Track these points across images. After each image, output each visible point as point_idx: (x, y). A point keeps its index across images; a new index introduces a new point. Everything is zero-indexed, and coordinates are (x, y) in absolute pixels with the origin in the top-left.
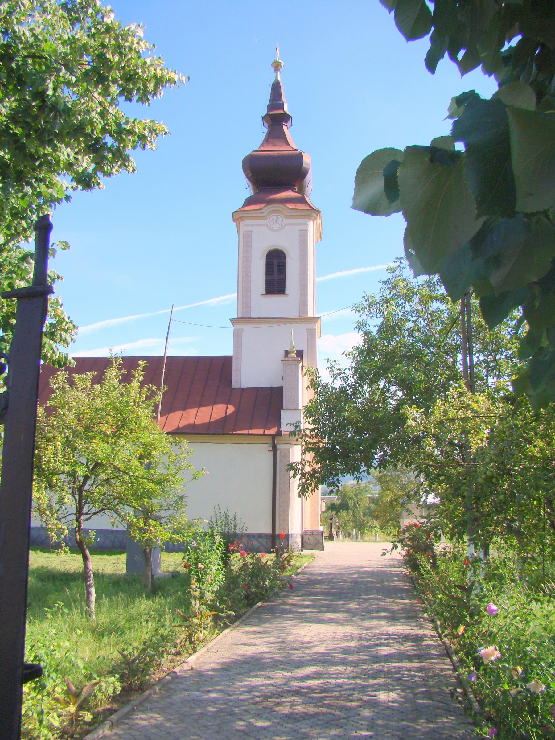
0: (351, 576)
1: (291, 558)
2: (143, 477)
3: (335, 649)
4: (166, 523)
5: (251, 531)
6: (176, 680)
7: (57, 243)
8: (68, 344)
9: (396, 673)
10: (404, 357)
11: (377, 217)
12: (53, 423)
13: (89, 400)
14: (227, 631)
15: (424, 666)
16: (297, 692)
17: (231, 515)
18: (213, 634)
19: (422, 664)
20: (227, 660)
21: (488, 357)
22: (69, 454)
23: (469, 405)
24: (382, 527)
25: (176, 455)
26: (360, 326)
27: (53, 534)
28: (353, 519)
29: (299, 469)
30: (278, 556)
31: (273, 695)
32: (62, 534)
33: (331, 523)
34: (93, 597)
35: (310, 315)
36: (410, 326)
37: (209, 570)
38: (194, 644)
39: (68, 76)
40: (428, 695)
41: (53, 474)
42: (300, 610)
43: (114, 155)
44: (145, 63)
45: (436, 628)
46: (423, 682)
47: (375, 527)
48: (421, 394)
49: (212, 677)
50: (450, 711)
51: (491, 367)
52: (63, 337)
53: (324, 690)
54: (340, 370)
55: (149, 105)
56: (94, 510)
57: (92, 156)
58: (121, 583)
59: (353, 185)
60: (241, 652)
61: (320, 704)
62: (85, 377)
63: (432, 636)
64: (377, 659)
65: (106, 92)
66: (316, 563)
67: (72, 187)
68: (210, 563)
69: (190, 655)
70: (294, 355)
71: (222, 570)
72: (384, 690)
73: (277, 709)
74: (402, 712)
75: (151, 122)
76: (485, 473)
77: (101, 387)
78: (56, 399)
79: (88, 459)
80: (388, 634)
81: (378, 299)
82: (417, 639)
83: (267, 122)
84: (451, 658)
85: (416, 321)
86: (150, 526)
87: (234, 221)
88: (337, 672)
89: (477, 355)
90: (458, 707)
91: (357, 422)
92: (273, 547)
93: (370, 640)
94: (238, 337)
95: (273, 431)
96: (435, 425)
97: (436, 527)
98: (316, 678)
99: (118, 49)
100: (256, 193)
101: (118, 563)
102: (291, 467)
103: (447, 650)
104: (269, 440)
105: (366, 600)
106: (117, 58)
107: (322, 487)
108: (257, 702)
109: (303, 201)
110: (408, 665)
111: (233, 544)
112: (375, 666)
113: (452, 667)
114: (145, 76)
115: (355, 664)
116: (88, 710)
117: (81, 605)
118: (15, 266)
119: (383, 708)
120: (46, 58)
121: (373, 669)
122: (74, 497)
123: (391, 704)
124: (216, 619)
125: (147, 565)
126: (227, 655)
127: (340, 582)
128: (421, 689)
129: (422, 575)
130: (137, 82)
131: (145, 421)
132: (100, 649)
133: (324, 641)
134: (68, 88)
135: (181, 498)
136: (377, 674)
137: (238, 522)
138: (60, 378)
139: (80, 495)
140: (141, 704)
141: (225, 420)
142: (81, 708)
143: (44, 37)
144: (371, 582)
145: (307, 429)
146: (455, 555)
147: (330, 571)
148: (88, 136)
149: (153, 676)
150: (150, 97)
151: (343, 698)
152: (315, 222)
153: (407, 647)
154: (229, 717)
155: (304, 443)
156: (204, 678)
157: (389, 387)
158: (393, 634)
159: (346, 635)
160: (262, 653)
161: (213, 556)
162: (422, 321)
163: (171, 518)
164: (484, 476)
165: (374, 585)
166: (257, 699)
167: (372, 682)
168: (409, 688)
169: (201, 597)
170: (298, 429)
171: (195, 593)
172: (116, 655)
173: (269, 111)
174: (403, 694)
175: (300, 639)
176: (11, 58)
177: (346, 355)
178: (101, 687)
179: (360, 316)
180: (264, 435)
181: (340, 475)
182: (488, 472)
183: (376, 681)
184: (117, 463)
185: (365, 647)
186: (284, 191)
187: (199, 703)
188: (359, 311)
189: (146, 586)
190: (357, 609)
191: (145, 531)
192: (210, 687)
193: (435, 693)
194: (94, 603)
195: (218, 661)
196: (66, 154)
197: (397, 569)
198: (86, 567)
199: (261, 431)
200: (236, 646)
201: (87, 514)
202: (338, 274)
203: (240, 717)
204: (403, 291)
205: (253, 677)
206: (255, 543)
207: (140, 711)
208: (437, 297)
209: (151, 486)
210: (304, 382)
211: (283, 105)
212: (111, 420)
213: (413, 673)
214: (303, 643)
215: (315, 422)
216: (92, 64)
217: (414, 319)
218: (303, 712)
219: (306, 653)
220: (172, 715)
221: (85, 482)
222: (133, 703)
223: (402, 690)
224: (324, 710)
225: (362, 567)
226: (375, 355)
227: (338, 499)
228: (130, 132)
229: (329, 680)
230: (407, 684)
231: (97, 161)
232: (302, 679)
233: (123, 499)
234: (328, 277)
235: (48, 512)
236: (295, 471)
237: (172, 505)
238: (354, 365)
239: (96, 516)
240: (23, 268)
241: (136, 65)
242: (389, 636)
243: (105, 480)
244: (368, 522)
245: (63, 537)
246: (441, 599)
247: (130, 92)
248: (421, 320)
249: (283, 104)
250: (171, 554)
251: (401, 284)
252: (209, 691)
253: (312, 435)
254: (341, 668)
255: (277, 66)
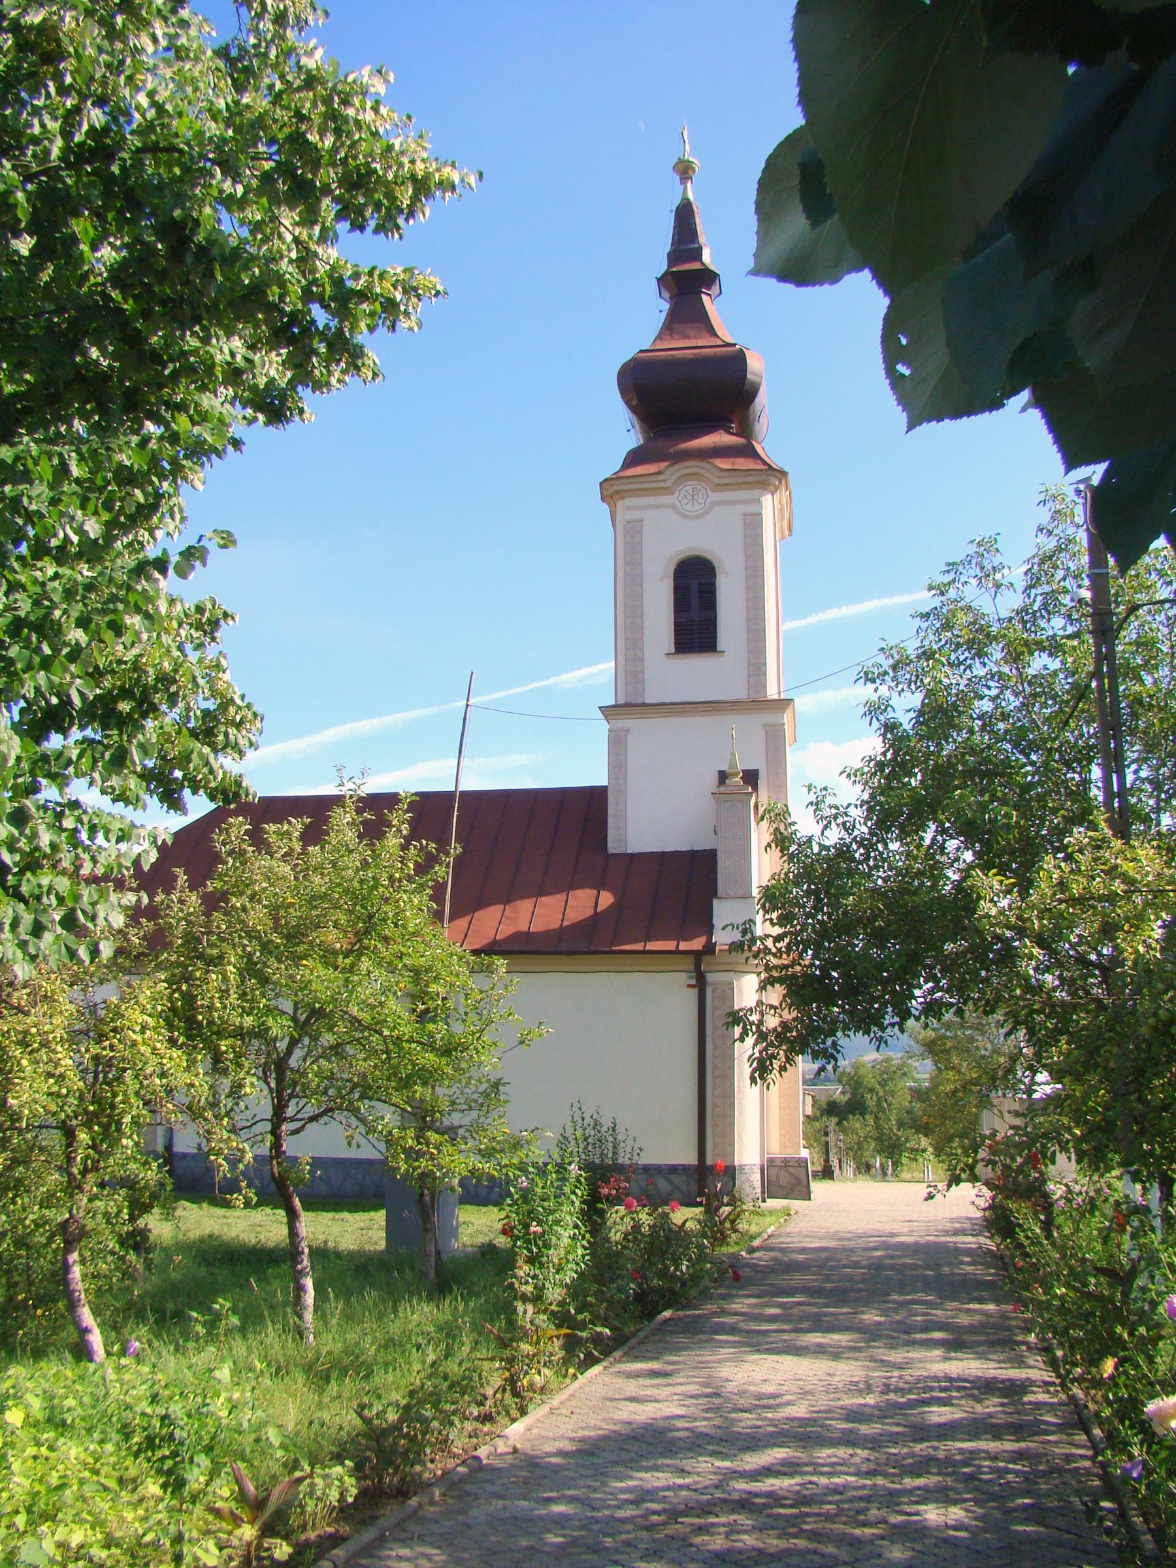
0: (867, 1254)
1: (738, 1216)
2: (411, 1040)
3: (829, 1411)
4: (463, 1137)
5: (648, 1158)
6: (480, 1475)
7: (209, 534)
8: (241, 754)
9: (965, 1463)
10: (969, 773)
11: (810, 288)
12: (218, 927)
13: (296, 879)
14: (596, 1369)
15: (1028, 1449)
16: (744, 1504)
17: (606, 1123)
18: (565, 1376)
19: (1023, 1445)
20: (592, 1433)
21: (1158, 770)
22: (253, 990)
23: (1116, 867)
24: (938, 1151)
25: (481, 992)
26: (874, 710)
27: (220, 1161)
28: (874, 1133)
29: (752, 1024)
30: (711, 1210)
31: (688, 1510)
32: (240, 1161)
33: (827, 1143)
34: (310, 1297)
35: (772, 692)
36: (985, 709)
37: (554, 1239)
38: (522, 1398)
39: (228, 186)
40: (1035, 1514)
41: (219, 1034)
42: (754, 1327)
43: (330, 346)
44: (390, 148)
45: (1053, 1363)
46: (1024, 1486)
47: (924, 1151)
48: (1012, 853)
49: (556, 1469)
50: (1086, 1553)
51: (1166, 792)
52: (232, 738)
53: (802, 1500)
54: (836, 808)
55: (401, 237)
56: (309, 1111)
57: (284, 351)
58: (371, 1268)
59: (752, 222)
60: (624, 1416)
61: (792, 1530)
62: (286, 827)
63: (1047, 1384)
64: (922, 1432)
65: (310, 217)
66: (791, 1227)
67: (244, 418)
68: (557, 1222)
69: (514, 1420)
70: (738, 780)
71: (583, 1237)
72: (937, 1501)
73: (697, 1540)
74: (978, 1552)
75: (404, 271)
76: (1155, 1015)
77: (323, 848)
78: (226, 875)
79: (296, 1004)
80: (949, 1379)
81: (912, 653)
82: (1013, 1390)
83: (669, 291)
84: (1088, 1433)
85: (997, 697)
86: (427, 1144)
87: (603, 499)
88: (834, 1459)
89: (1134, 767)
90: (1106, 1544)
91: (874, 918)
92: (701, 1193)
93: (910, 1391)
94: (617, 745)
95: (697, 944)
96: (1041, 912)
97: (1045, 1135)
98: (785, 1474)
99: (335, 122)
100: (648, 440)
101: (369, 1229)
102: (735, 1018)
103: (1079, 1414)
104: (689, 963)
105: (901, 1305)
106: (329, 141)
107: (804, 1065)
108: (653, 1525)
109: (749, 452)
110: (993, 1446)
111: (607, 1182)
112: (918, 1448)
113: (1090, 1453)
114: (390, 176)
115: (874, 1443)
116: (286, 1537)
117: (285, 1314)
118: (120, 587)
119: (933, 1541)
120: (181, 152)
121: (912, 1455)
122: (268, 1084)
123: (952, 1533)
124: (571, 1344)
125: (426, 1230)
126: (592, 1422)
127: (845, 1267)
128: (1020, 1501)
129: (1020, 1246)
130: (375, 190)
131: (414, 921)
132: (320, 1405)
133: (806, 1393)
134: (229, 210)
135: (496, 1085)
136: (922, 1466)
137: (620, 1137)
138: (234, 832)
139: (280, 1080)
140: (400, 1524)
141: (594, 922)
142: (268, 1530)
143: (177, 106)
144: (914, 1267)
145: (767, 936)
146: (1092, 1199)
147: (824, 1244)
148: (273, 308)
149: (430, 1465)
150: (401, 221)
151: (844, 1519)
152: (777, 496)
153: (991, 1406)
154: (589, 1557)
155: (761, 969)
156: (539, 1472)
157: (944, 841)
158: (959, 1379)
159: (855, 1379)
160: (668, 1418)
161: (564, 1208)
162: (1012, 698)
163: (474, 1129)
164: (1151, 1021)
165: (919, 1272)
166: (655, 1518)
167: (909, 1482)
168: (994, 1497)
169: (537, 1298)
170: (749, 936)
171: (523, 1288)
172: (350, 1420)
173: (670, 265)
174: (979, 1510)
175: (752, 1388)
176: (109, 155)
177: (849, 776)
178: (312, 1486)
179: (876, 690)
180: (677, 952)
181: (839, 1034)
182: (1160, 1012)
183: (920, 1482)
184: (354, 1010)
185: (897, 1406)
186: (709, 433)
187: (524, 1525)
188: (873, 681)
189: (423, 1275)
190: (879, 1323)
191: (419, 1155)
192: (552, 1490)
193: (1052, 1509)
194: (311, 1309)
195: (573, 1435)
196: (226, 350)
197: (970, 1239)
198: (293, 1233)
199: (670, 945)
200: (614, 1404)
201: (292, 1119)
202: (832, 614)
203: (614, 1558)
204: (966, 635)
205: (647, 1469)
206: (662, 1184)
207: (396, 1540)
208: (1042, 642)
209: (429, 1058)
210: (760, 835)
211: (699, 250)
212: (343, 919)
213: (1001, 1464)
214: (760, 1396)
215: (783, 920)
216: (277, 158)
217: (994, 692)
218: (754, 1549)
219: (765, 1419)
220: (465, 1550)
221: (289, 1052)
222: (383, 1522)
223: (977, 1502)
224: (801, 1543)
225: (893, 1235)
226: (912, 775)
227: (842, 1093)
228: (363, 295)
229: (814, 1479)
230: (989, 1488)
231: (297, 361)
232: (756, 1475)
233: (370, 1088)
234: (812, 619)
235: (209, 1115)
236: (744, 1028)
237: (476, 1101)
238: (866, 796)
239: (314, 1124)
240: (139, 588)
241: (371, 154)
242: (952, 1382)
243: (331, 1048)
244: (907, 1140)
245: (241, 1166)
246: (1062, 1298)
247: (360, 211)
248: (1008, 694)
249: (700, 249)
250: (484, 1209)
251: (963, 618)
252: (550, 1500)
253: (779, 950)
254: (842, 1452)
255: (684, 171)
